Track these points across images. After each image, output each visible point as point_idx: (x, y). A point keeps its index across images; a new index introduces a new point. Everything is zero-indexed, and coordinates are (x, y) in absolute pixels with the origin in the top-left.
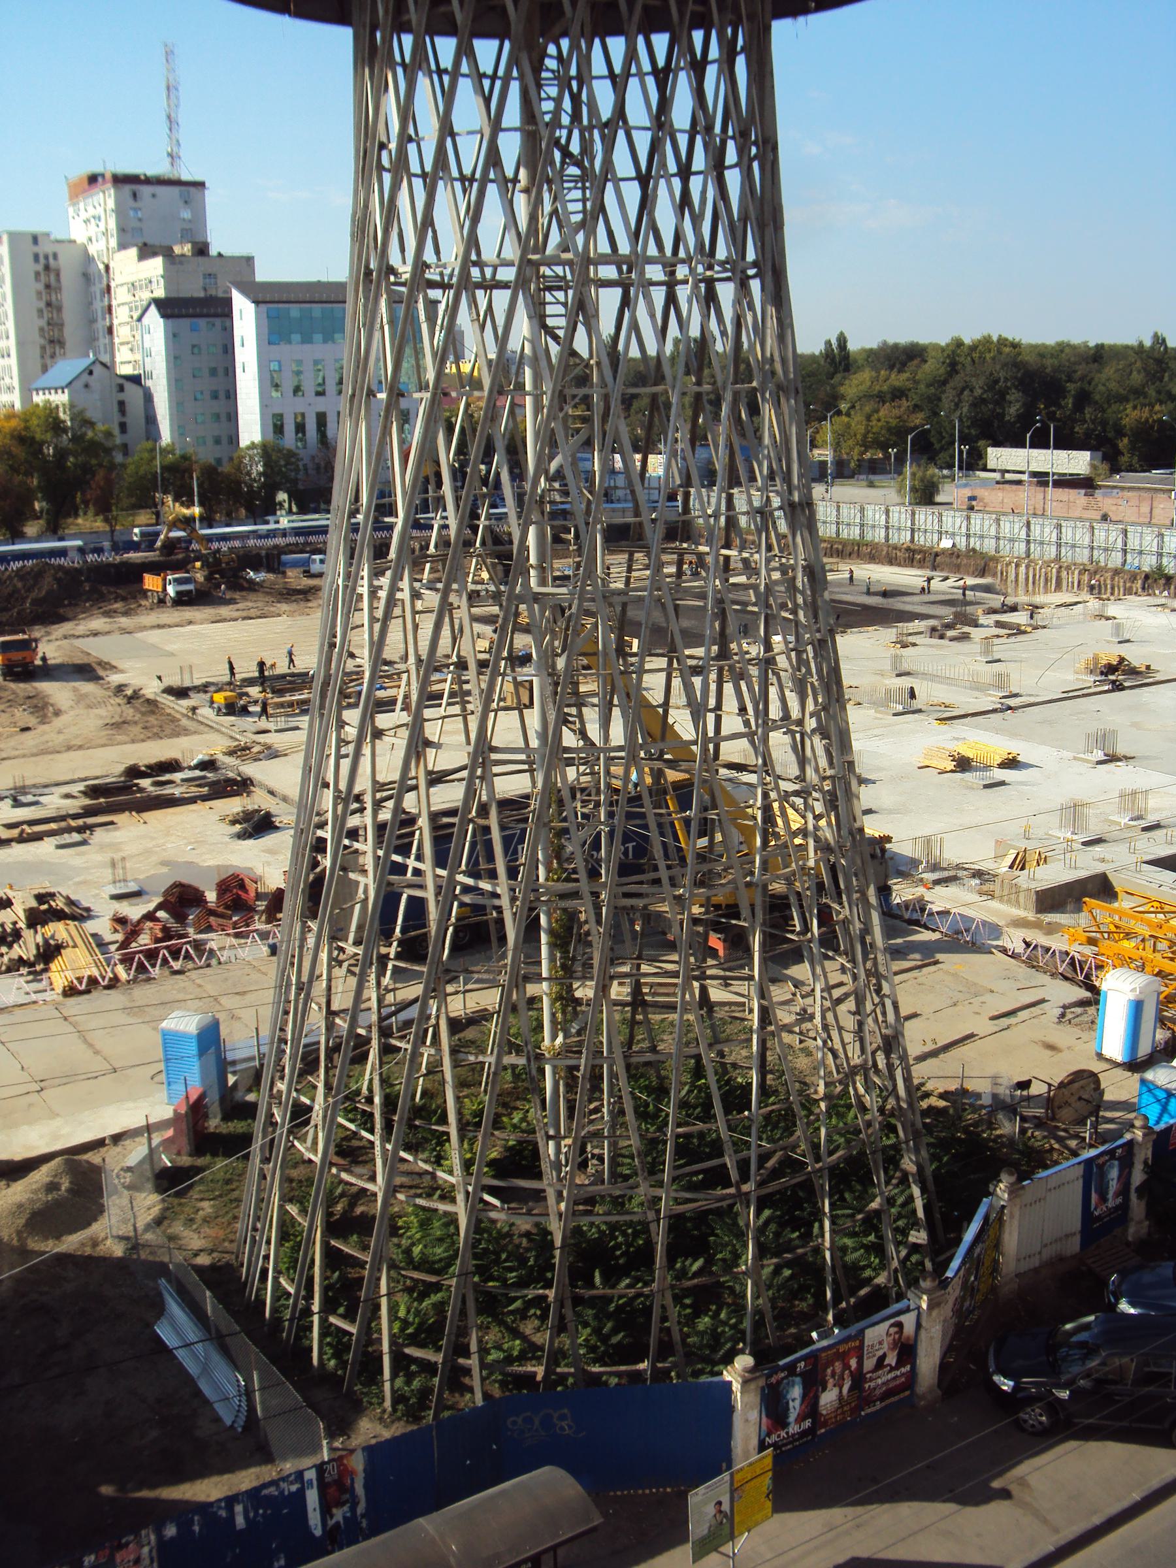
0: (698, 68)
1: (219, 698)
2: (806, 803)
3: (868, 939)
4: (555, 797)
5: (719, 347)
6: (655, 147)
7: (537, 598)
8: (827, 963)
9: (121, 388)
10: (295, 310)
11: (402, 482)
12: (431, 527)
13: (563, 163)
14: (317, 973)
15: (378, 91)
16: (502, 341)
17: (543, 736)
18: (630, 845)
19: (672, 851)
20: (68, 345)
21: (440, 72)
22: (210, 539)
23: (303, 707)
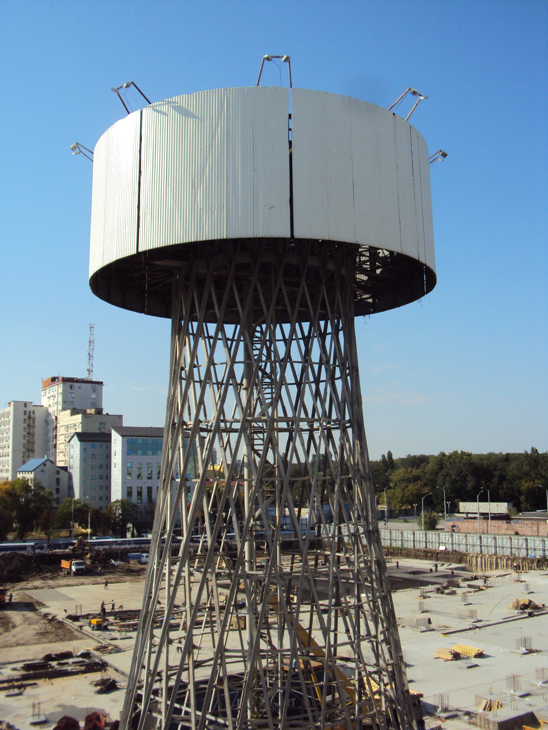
0: (322, 336)
1: (94, 621)
5: (333, 458)
6: (304, 370)
7: (248, 576)
9: (58, 473)
10: (140, 440)
11: (186, 520)
12: (199, 542)
13: (263, 377)
16: (234, 456)
17: (250, 643)
18: (293, 700)
19: (314, 704)
20: (35, 452)
21: (209, 337)
23: (134, 627)
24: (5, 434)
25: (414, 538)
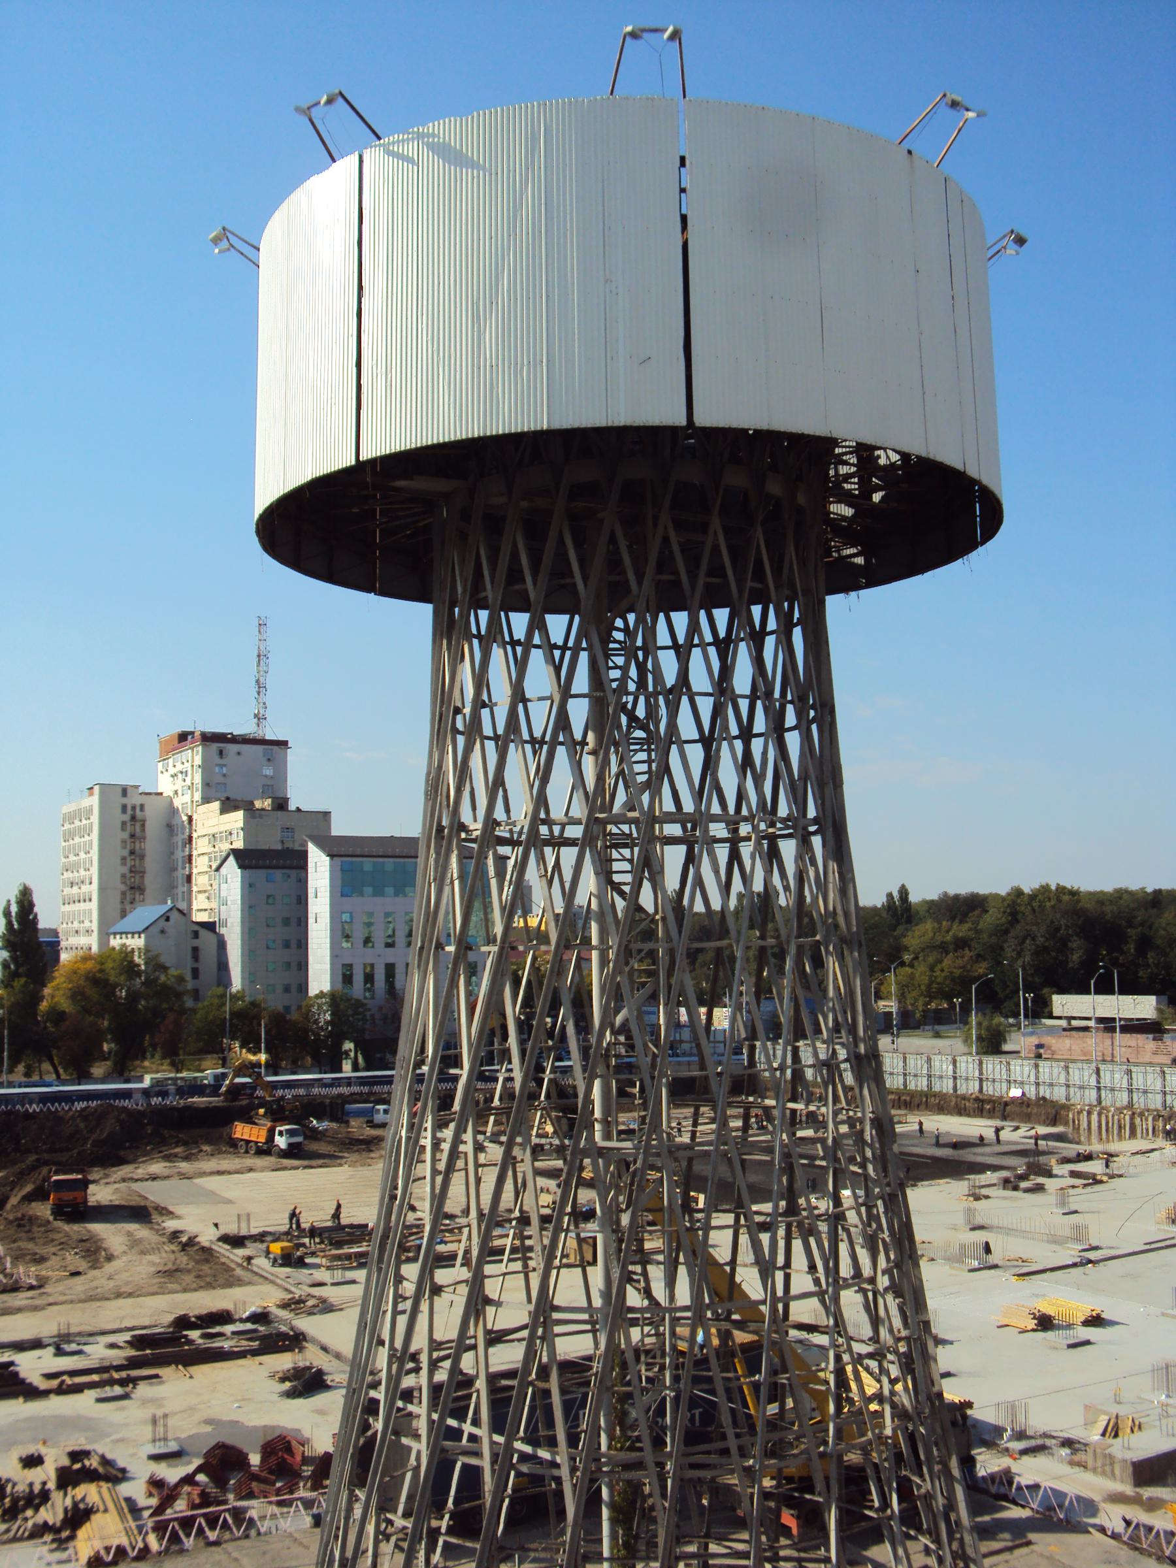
0: (757, 639)
1: (276, 1248)
2: (881, 1366)
3: (953, 1516)
4: (618, 1359)
5: (782, 901)
7: (601, 1152)
8: (909, 1544)
9: (196, 935)
10: (368, 864)
11: (468, 1033)
12: (497, 1080)
13: (629, 726)
14: (363, 1547)
15: (455, 660)
16: (569, 897)
17: (606, 1294)
18: (697, 1412)
19: (741, 1420)
20: (147, 892)
21: (514, 643)
22: (274, 1086)
23: (361, 1261)
24: (82, 855)
25: (955, 1072)
